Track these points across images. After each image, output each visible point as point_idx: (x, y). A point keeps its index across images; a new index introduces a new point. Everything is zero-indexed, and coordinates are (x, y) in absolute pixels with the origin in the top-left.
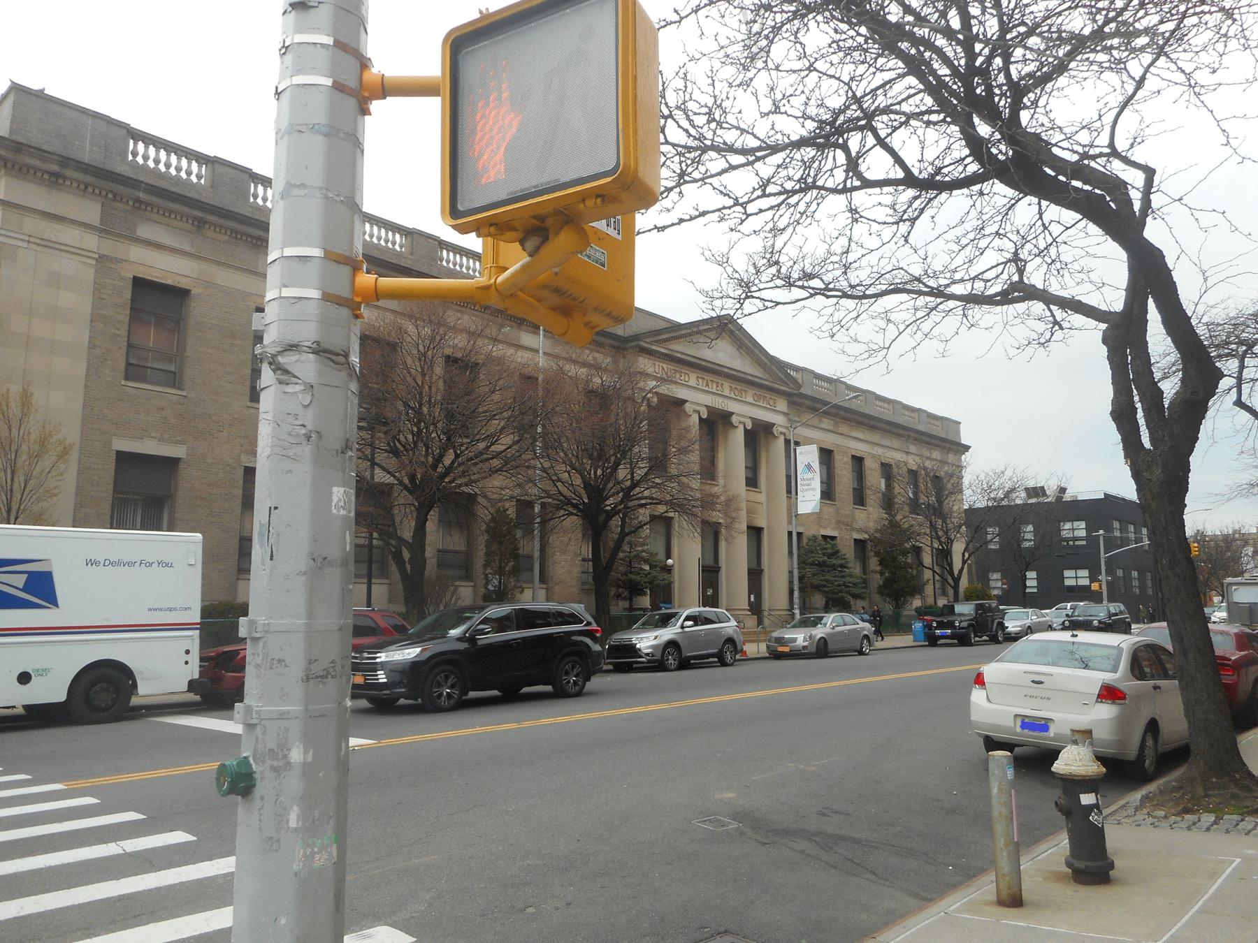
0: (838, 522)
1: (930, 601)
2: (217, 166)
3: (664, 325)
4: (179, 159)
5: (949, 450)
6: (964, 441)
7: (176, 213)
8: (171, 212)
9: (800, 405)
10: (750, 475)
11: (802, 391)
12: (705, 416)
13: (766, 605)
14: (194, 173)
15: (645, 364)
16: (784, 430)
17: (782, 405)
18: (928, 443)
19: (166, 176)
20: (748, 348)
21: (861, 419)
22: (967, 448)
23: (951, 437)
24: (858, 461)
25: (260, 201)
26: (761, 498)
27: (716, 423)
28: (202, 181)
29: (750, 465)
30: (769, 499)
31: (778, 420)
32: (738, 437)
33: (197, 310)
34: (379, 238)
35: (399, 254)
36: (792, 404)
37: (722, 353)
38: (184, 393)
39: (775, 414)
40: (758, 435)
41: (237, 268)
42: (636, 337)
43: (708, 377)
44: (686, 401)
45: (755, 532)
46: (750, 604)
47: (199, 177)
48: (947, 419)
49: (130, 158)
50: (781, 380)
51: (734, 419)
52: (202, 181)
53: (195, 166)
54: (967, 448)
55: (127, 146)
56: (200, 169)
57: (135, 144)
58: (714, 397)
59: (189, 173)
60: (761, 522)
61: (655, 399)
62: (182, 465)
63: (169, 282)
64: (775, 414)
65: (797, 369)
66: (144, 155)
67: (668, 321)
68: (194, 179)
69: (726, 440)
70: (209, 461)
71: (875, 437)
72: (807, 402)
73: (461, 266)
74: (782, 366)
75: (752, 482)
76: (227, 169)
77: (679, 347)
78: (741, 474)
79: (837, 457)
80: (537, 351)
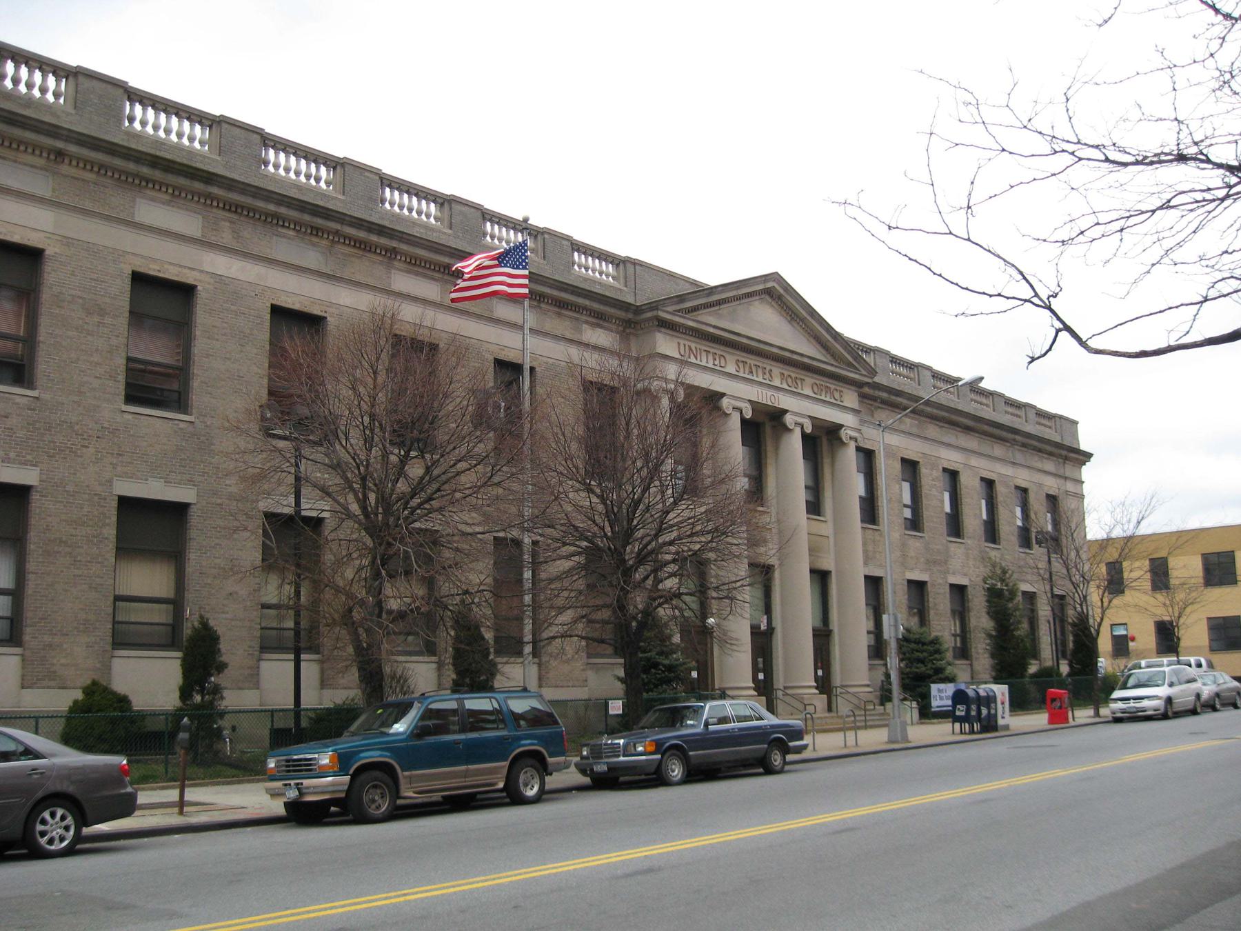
0: (928, 562)
1: (1049, 663)
2: (81, 79)
3: (689, 289)
4: (31, 72)
5: (1066, 458)
6: (1084, 446)
7: (27, 144)
8: (20, 143)
9: (874, 399)
10: (811, 499)
11: (877, 379)
12: (748, 414)
13: (837, 679)
14: (192, 138)
15: (666, 344)
16: (854, 434)
17: (851, 398)
18: (1040, 451)
19: (28, 101)
20: (803, 320)
21: (970, 423)
22: (1088, 456)
23: (1067, 442)
24: (953, 476)
25: (137, 125)
26: (826, 528)
27: (762, 427)
28: (62, 101)
29: (810, 483)
30: (838, 530)
31: (846, 419)
32: (794, 443)
33: (53, 277)
34: (287, 170)
35: (323, 195)
36: (863, 396)
37: (763, 323)
38: (35, 393)
39: (843, 413)
40: (821, 441)
41: (107, 218)
42: (654, 306)
43: (752, 360)
44: (723, 395)
45: (821, 577)
46: (817, 679)
47: (57, 95)
48: (1061, 417)
49: (127, 124)
50: (850, 364)
51: (789, 419)
52: (62, 101)
53: (51, 80)
54: (1088, 456)
55: (122, 108)
56: (58, 84)
57: (132, 106)
58: (760, 389)
59: (43, 90)
60: (827, 563)
61: (681, 392)
62: (35, 497)
63: (16, 239)
64: (843, 413)
65: (869, 350)
66: (144, 121)
67: (694, 283)
68: (50, 97)
69: (777, 448)
70: (70, 488)
71: (971, 442)
72: (884, 395)
73: (410, 210)
74: (856, 352)
75: (814, 507)
76: (95, 83)
77: (711, 320)
78: (800, 497)
79: (924, 471)
80: (522, 328)
